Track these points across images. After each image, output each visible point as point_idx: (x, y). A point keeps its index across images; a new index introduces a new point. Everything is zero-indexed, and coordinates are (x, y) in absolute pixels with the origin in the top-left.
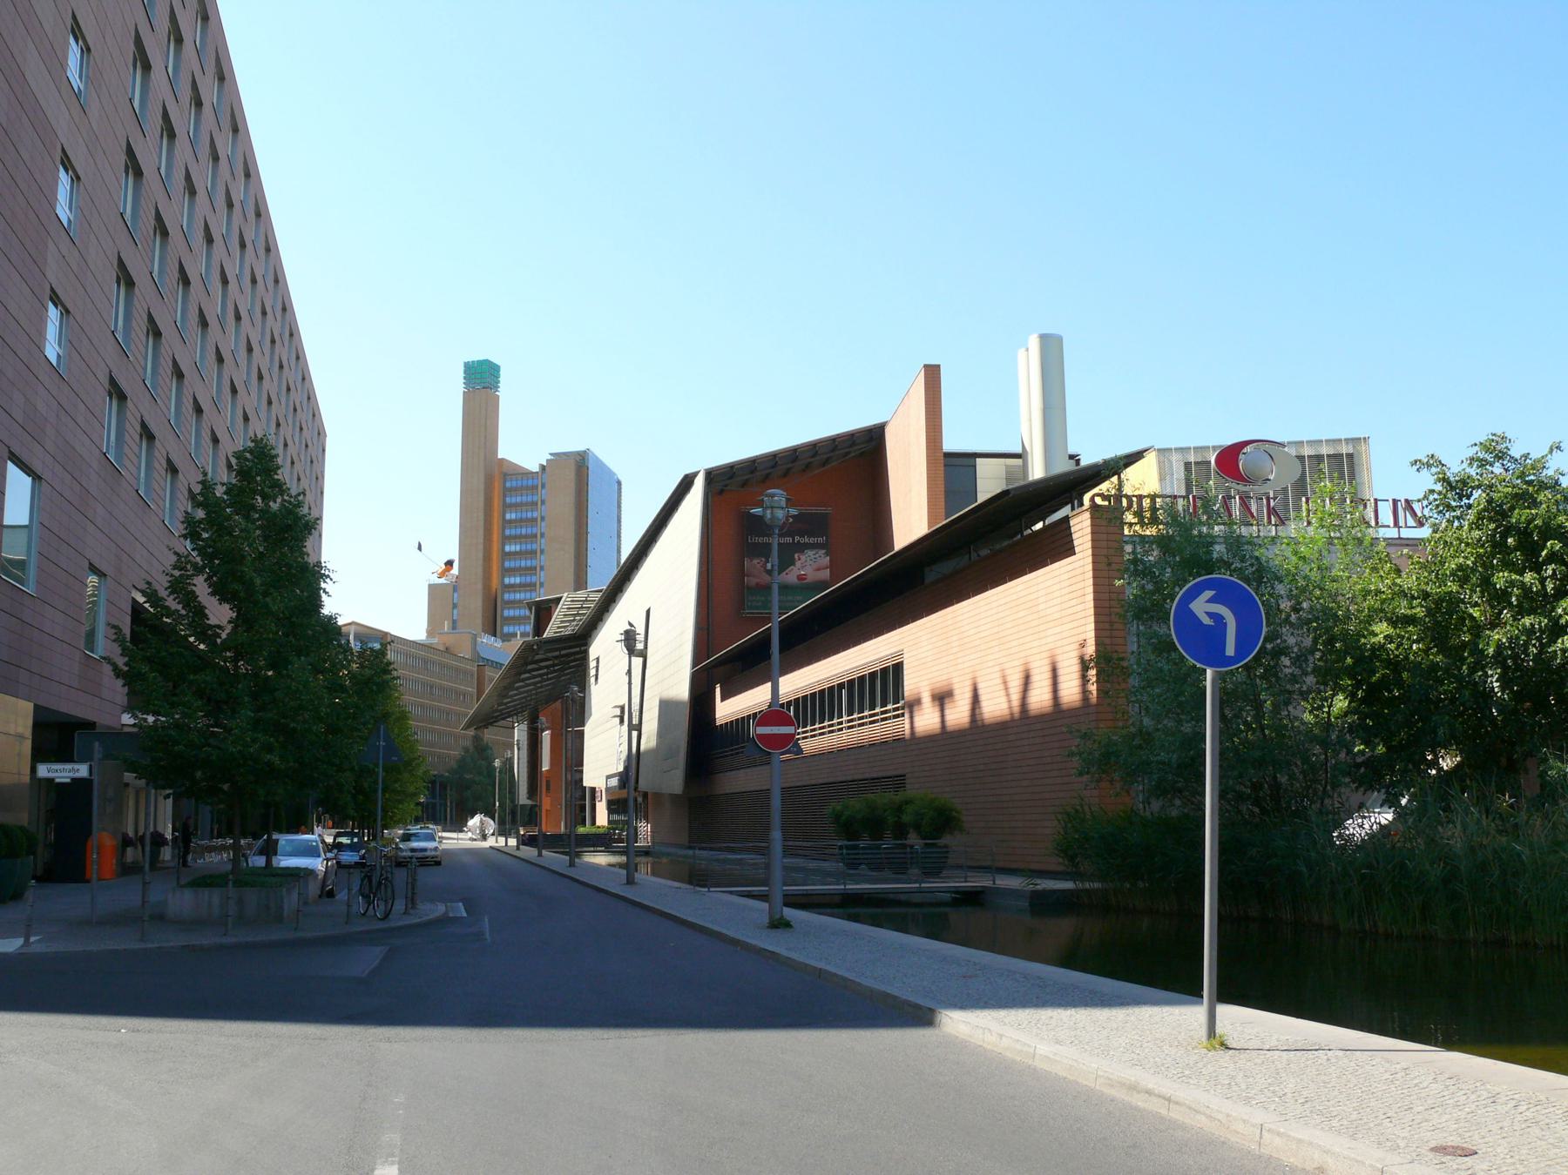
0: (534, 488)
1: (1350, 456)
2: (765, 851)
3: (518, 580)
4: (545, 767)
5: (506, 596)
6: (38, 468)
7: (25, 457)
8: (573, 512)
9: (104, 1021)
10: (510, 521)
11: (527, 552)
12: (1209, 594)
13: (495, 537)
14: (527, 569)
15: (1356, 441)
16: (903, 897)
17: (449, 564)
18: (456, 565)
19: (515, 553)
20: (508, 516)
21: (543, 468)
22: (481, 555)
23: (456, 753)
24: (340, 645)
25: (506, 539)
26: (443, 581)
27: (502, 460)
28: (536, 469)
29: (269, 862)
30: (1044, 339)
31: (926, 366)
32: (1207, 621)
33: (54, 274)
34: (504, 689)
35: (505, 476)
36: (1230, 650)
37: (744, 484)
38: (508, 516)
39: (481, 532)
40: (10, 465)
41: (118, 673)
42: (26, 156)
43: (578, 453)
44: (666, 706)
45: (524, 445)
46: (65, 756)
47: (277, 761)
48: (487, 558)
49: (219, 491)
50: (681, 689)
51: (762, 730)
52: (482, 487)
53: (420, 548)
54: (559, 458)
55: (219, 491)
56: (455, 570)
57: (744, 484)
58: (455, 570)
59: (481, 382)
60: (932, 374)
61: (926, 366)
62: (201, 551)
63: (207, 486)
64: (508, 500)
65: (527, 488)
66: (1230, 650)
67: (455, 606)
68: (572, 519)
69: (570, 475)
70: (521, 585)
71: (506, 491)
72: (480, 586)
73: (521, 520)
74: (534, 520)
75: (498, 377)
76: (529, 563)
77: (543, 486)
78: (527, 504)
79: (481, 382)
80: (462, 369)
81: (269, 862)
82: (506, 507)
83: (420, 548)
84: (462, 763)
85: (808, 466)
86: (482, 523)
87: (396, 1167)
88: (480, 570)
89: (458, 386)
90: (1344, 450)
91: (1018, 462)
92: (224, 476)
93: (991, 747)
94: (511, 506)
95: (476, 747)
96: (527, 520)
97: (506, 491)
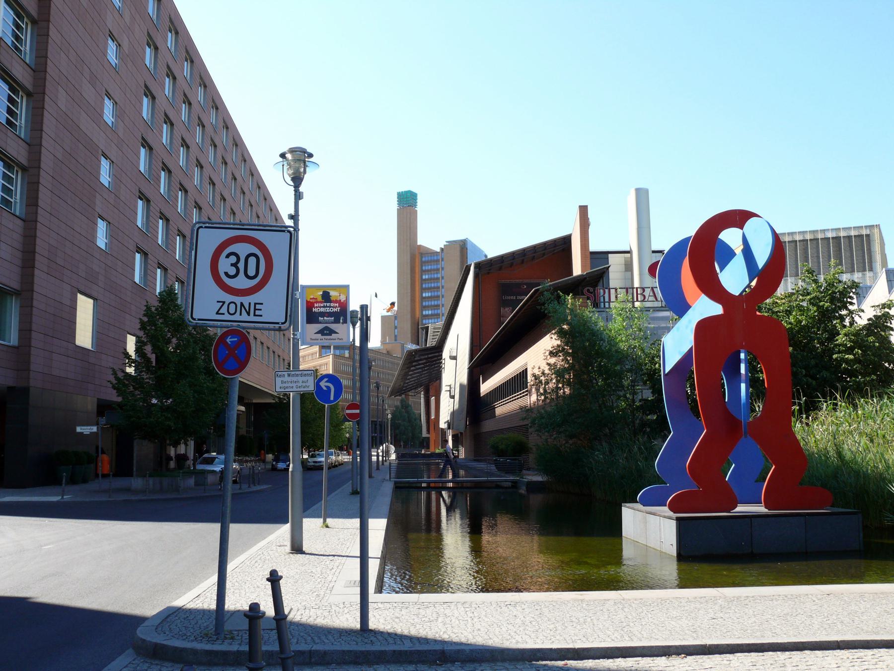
0: (438, 261)
1: (868, 236)
3: (430, 312)
4: (433, 417)
6: (95, 294)
7: (88, 292)
9: (38, 519)
10: (425, 280)
11: (434, 297)
12: (326, 380)
13: (417, 288)
15: (871, 227)
16: (465, 485)
17: (393, 304)
18: (396, 305)
19: (428, 297)
20: (424, 277)
21: (442, 249)
22: (409, 298)
25: (423, 290)
26: (389, 314)
27: (420, 246)
28: (438, 250)
30: (638, 190)
31: (580, 207)
32: (325, 388)
33: (98, 210)
34: (404, 375)
35: (422, 255)
36: (332, 398)
37: (500, 268)
38: (424, 277)
39: (409, 287)
40: (79, 295)
41: (114, 388)
42: (82, 162)
43: (462, 241)
44: (461, 386)
45: (432, 236)
47: (172, 424)
48: (413, 300)
49: (153, 309)
50: (464, 378)
51: (348, 411)
54: (451, 244)
55: (153, 309)
56: (396, 308)
57: (500, 268)
58: (396, 308)
59: (407, 203)
60: (642, 196)
61: (580, 207)
62: (147, 335)
63: (148, 308)
65: (434, 261)
66: (332, 398)
67: (396, 328)
69: (457, 253)
70: (432, 315)
71: (423, 263)
72: (409, 316)
73: (431, 279)
74: (438, 279)
75: (416, 200)
76: (436, 303)
77: (442, 260)
78: (434, 270)
79: (407, 203)
80: (396, 196)
82: (423, 272)
85: (533, 258)
88: (409, 308)
89: (393, 206)
90: (864, 232)
91: (628, 255)
92: (157, 304)
95: (402, 406)
96: (434, 279)
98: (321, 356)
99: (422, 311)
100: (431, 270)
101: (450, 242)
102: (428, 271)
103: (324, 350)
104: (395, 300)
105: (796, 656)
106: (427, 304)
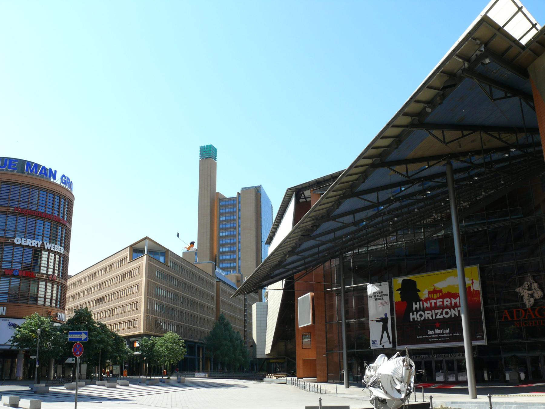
2: (473, 349)
3: (227, 249)
5: (221, 258)
8: (254, 214)
11: (231, 236)
14: (231, 244)
17: (192, 243)
19: (225, 236)
21: (239, 194)
22: (209, 237)
23: (207, 330)
24: (61, 330)
25: (220, 230)
27: (218, 193)
28: (235, 195)
29: (76, 392)
39: (209, 226)
43: (256, 187)
45: (228, 187)
46: (352, 349)
48: (212, 239)
52: (209, 204)
53: (178, 236)
56: (196, 246)
58: (196, 246)
59: (208, 155)
64: (221, 211)
68: (254, 218)
69: (253, 196)
70: (228, 252)
72: (208, 252)
78: (231, 212)
79: (208, 155)
80: (199, 150)
81: (76, 392)
82: (220, 214)
83: (178, 236)
84: (214, 333)
86: (209, 221)
87: (42, 403)
88: (208, 245)
93: (123, 346)
94: (223, 214)
97: (220, 207)
98: (132, 259)
99: (219, 249)
100: (228, 260)
101: (244, 189)
102: (225, 213)
103: (135, 254)
104: (195, 239)
105: (452, 139)
106: (224, 258)
